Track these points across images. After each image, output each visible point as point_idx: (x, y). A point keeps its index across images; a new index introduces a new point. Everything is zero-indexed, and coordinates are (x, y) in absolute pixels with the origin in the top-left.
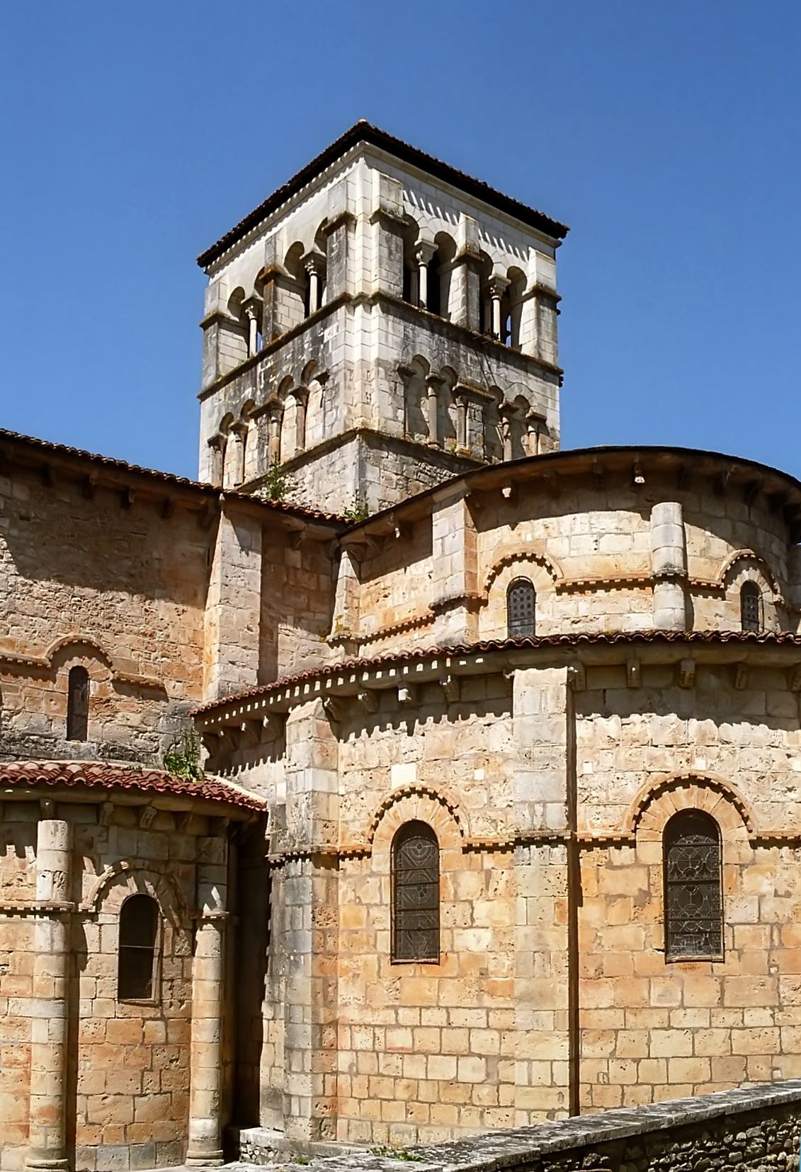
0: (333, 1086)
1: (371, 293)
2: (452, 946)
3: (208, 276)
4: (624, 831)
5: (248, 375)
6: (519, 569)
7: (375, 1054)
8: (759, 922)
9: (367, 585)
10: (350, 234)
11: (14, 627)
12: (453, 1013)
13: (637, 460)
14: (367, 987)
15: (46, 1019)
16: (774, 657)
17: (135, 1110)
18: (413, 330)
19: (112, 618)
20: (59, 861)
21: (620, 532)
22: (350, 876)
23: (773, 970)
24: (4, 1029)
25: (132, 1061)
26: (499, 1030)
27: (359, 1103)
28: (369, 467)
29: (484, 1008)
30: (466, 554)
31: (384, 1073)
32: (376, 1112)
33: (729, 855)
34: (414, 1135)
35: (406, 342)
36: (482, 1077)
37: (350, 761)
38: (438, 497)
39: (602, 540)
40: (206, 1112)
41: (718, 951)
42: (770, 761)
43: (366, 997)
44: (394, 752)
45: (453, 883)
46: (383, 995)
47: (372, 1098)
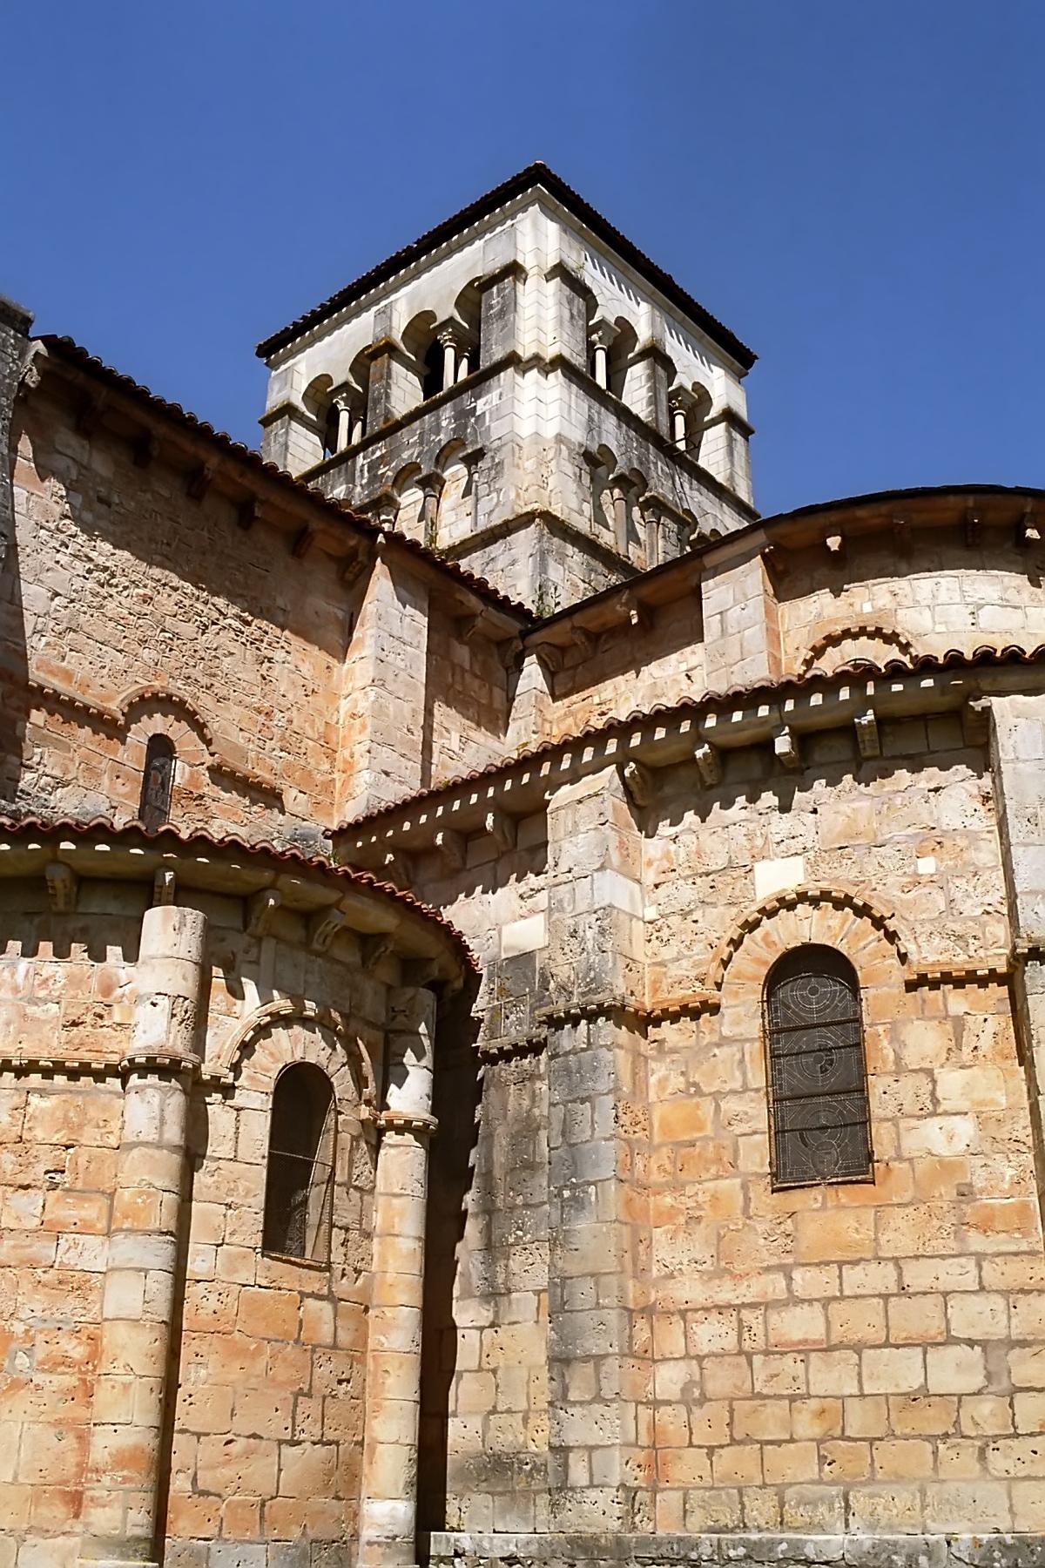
0: (648, 1429)
1: (549, 354)
2: (898, 1148)
3: (268, 368)
5: (339, 472)
7: (743, 1360)
9: (566, 701)
10: (520, 286)
11: (74, 653)
13: (1028, 510)
14: (720, 1238)
15: (141, 1270)
17: (280, 1470)
18: (599, 413)
19: (215, 675)
20: (184, 978)
21: (1005, 604)
22: (674, 1051)
24: (45, 1294)
25: (281, 1373)
26: (1005, 1293)
27: (710, 1455)
29: (971, 1254)
30: (767, 629)
31: (765, 1391)
32: (751, 1469)
34: (839, 1504)
35: (591, 426)
36: (978, 1381)
37: (666, 865)
40: (396, 1483)
43: (717, 1257)
44: (759, 842)
45: (890, 1043)
46: (759, 1245)
47: (740, 1443)
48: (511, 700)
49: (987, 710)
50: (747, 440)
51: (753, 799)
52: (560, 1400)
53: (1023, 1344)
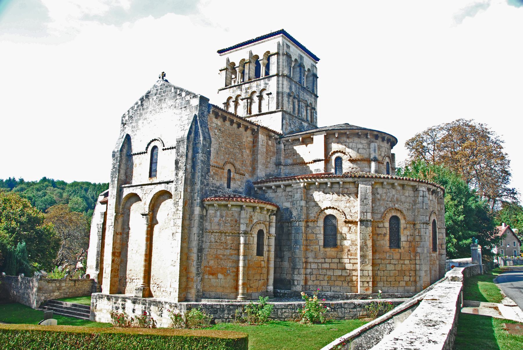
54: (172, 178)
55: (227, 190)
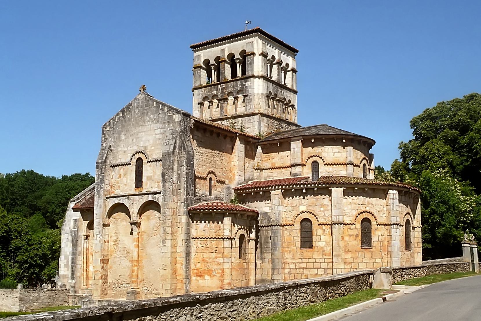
1: (260, 75)
4: (353, 222)
6: (315, 159)
8: (379, 241)
12: (316, 259)
13: (344, 137)
16: (382, 188)
21: (339, 152)
22: (288, 230)
23: (381, 251)
28: (261, 122)
33: (373, 227)
36: (323, 273)
38: (292, 139)
39: (335, 154)
41: (371, 247)
42: (380, 208)
43: (293, 257)
44: (300, 203)
46: (298, 256)
48: (256, 153)
49: (331, 190)
50: (296, 74)
51: (300, 197)
52: (273, 274)
53: (329, 269)
54: (160, 189)
55: (209, 197)
